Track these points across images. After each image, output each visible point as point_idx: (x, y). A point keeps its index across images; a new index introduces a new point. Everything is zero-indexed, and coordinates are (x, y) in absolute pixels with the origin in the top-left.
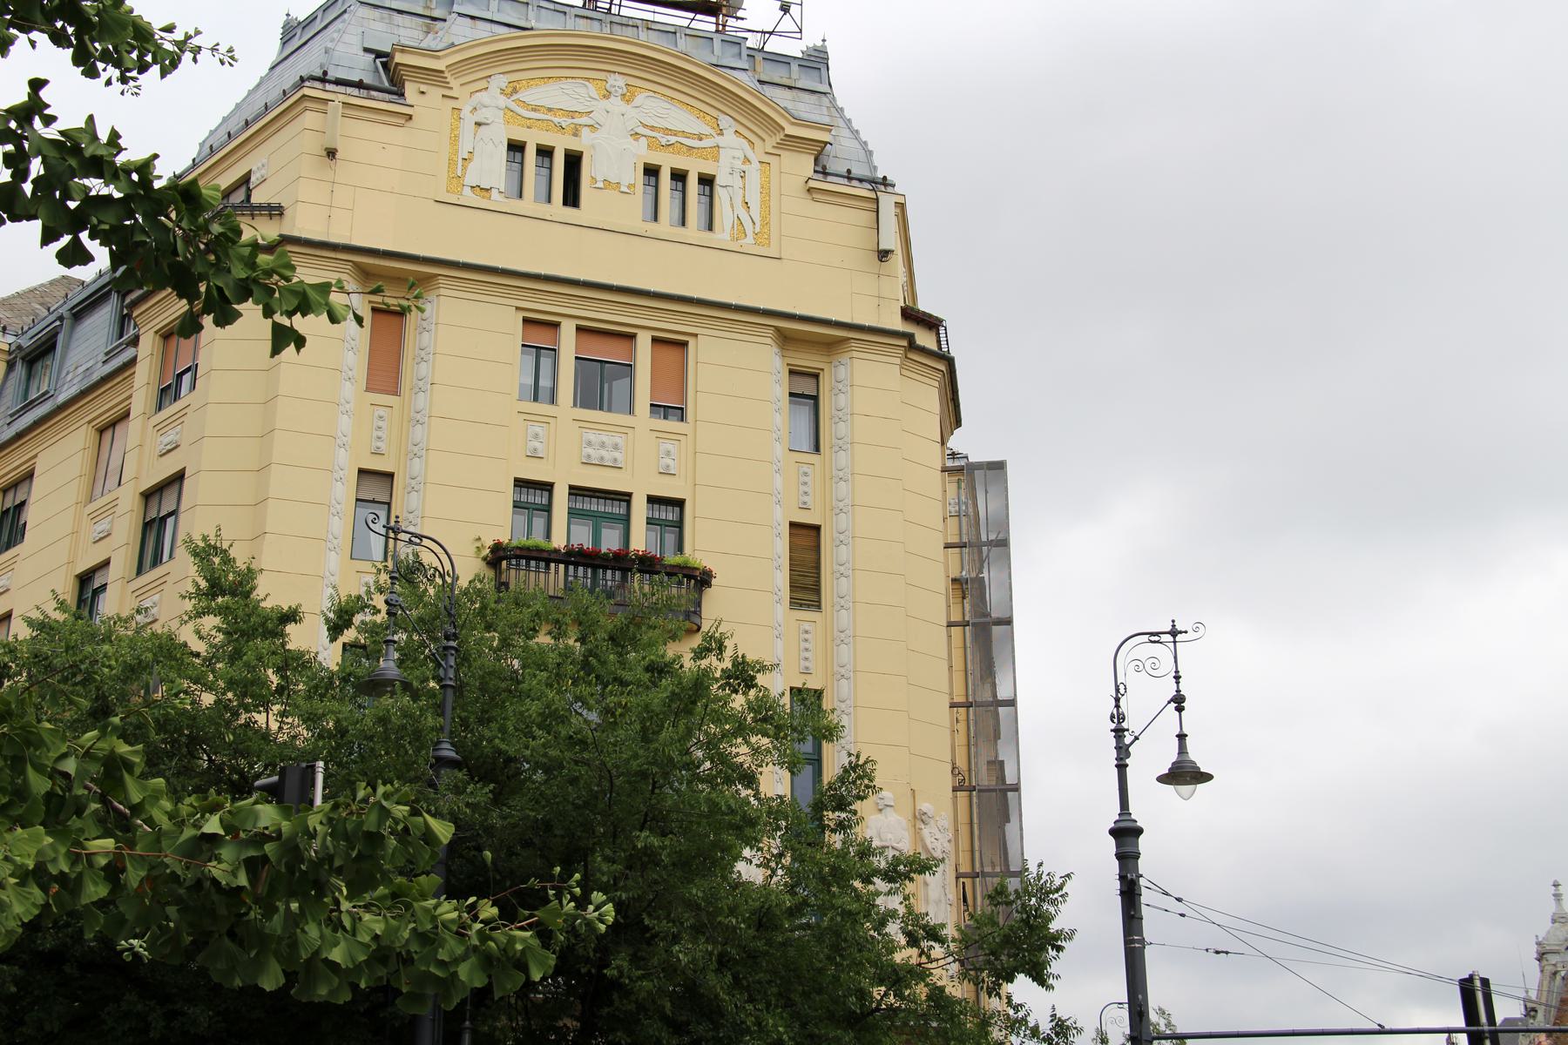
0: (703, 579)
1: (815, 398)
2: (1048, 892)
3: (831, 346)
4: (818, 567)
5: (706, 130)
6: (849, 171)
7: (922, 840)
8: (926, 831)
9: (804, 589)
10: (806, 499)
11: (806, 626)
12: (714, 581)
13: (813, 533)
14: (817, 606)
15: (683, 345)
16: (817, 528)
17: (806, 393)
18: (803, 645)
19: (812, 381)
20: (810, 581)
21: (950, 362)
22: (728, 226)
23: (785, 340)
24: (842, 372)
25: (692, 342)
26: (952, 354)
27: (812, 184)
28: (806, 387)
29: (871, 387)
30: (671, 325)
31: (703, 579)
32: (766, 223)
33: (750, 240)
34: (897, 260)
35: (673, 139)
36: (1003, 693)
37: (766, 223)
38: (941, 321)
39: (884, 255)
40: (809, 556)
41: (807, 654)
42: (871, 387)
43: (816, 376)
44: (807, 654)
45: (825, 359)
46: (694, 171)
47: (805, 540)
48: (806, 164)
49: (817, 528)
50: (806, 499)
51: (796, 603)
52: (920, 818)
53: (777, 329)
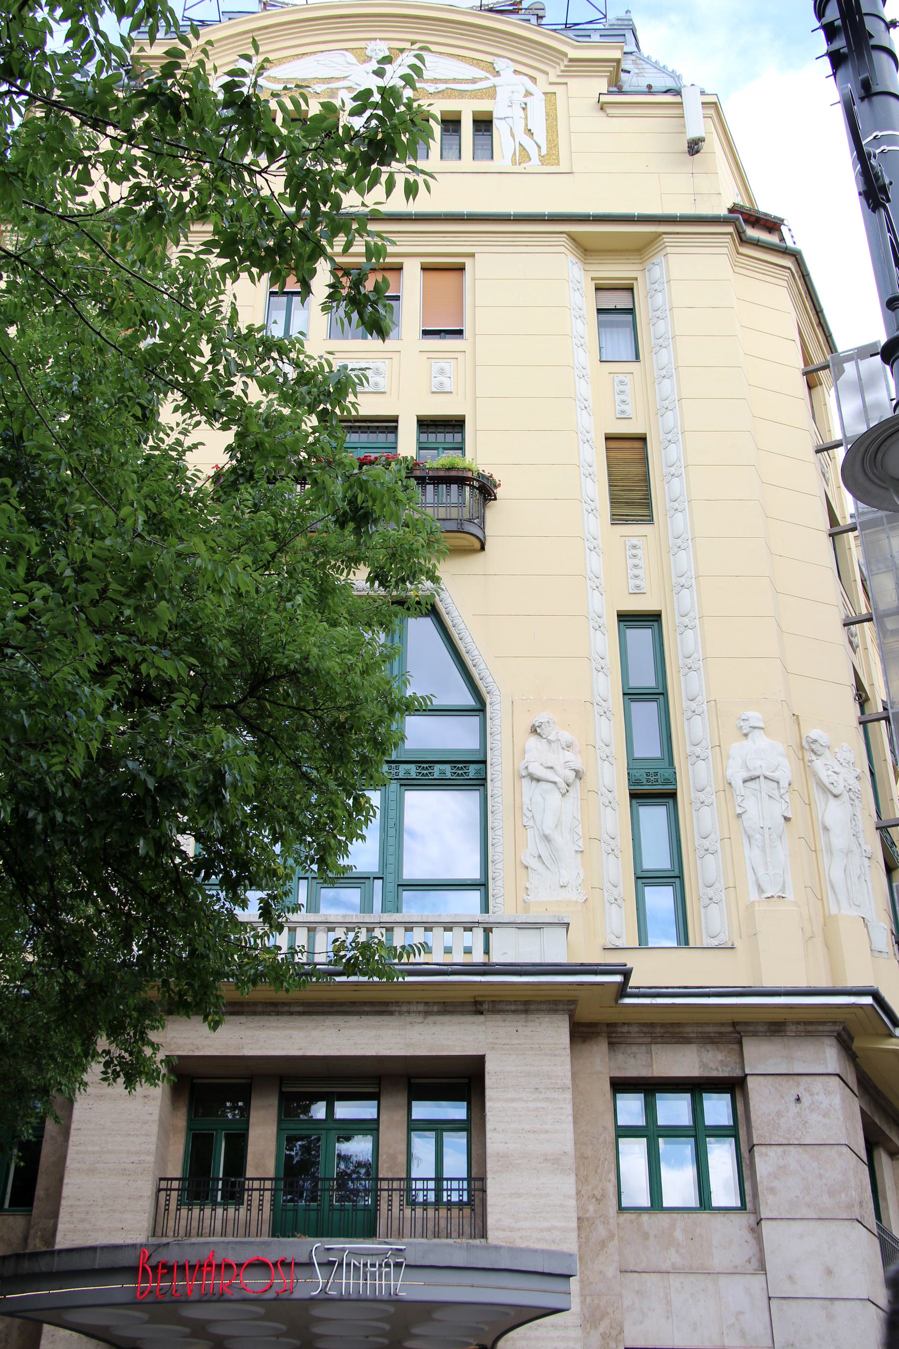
0: (486, 490)
1: (631, 311)
2: (214, 1026)
3: (641, 250)
4: (646, 479)
5: (479, 73)
6: (649, 87)
7: (815, 775)
8: (818, 764)
9: (630, 503)
10: (624, 407)
11: (635, 541)
12: (499, 492)
13: (638, 444)
14: (649, 519)
15: (461, 269)
16: (642, 439)
17: (618, 310)
18: (631, 562)
19: (626, 295)
20: (636, 496)
21: (796, 256)
22: (509, 154)
23: (586, 250)
24: (656, 272)
25: (468, 262)
26: (799, 246)
27: (604, 99)
28: (619, 300)
29: (694, 282)
30: (442, 244)
31: (486, 490)
32: (553, 143)
33: (535, 160)
34: (714, 145)
35: (442, 87)
36: (847, 71)
37: (553, 143)
38: (782, 220)
39: (694, 147)
40: (636, 470)
41: (637, 572)
42: (694, 282)
43: (631, 289)
44: (637, 572)
45: (639, 267)
46: (467, 111)
47: (629, 451)
48: (602, 85)
49: (642, 439)
50: (624, 407)
51: (617, 519)
52: (807, 749)
53: (568, 234)
